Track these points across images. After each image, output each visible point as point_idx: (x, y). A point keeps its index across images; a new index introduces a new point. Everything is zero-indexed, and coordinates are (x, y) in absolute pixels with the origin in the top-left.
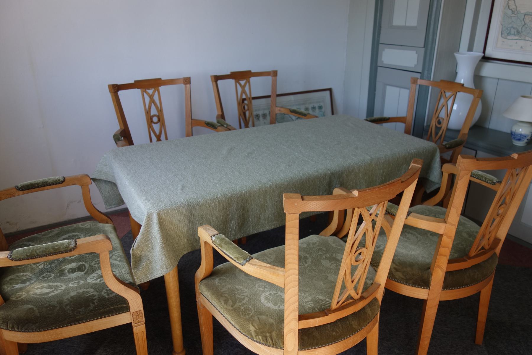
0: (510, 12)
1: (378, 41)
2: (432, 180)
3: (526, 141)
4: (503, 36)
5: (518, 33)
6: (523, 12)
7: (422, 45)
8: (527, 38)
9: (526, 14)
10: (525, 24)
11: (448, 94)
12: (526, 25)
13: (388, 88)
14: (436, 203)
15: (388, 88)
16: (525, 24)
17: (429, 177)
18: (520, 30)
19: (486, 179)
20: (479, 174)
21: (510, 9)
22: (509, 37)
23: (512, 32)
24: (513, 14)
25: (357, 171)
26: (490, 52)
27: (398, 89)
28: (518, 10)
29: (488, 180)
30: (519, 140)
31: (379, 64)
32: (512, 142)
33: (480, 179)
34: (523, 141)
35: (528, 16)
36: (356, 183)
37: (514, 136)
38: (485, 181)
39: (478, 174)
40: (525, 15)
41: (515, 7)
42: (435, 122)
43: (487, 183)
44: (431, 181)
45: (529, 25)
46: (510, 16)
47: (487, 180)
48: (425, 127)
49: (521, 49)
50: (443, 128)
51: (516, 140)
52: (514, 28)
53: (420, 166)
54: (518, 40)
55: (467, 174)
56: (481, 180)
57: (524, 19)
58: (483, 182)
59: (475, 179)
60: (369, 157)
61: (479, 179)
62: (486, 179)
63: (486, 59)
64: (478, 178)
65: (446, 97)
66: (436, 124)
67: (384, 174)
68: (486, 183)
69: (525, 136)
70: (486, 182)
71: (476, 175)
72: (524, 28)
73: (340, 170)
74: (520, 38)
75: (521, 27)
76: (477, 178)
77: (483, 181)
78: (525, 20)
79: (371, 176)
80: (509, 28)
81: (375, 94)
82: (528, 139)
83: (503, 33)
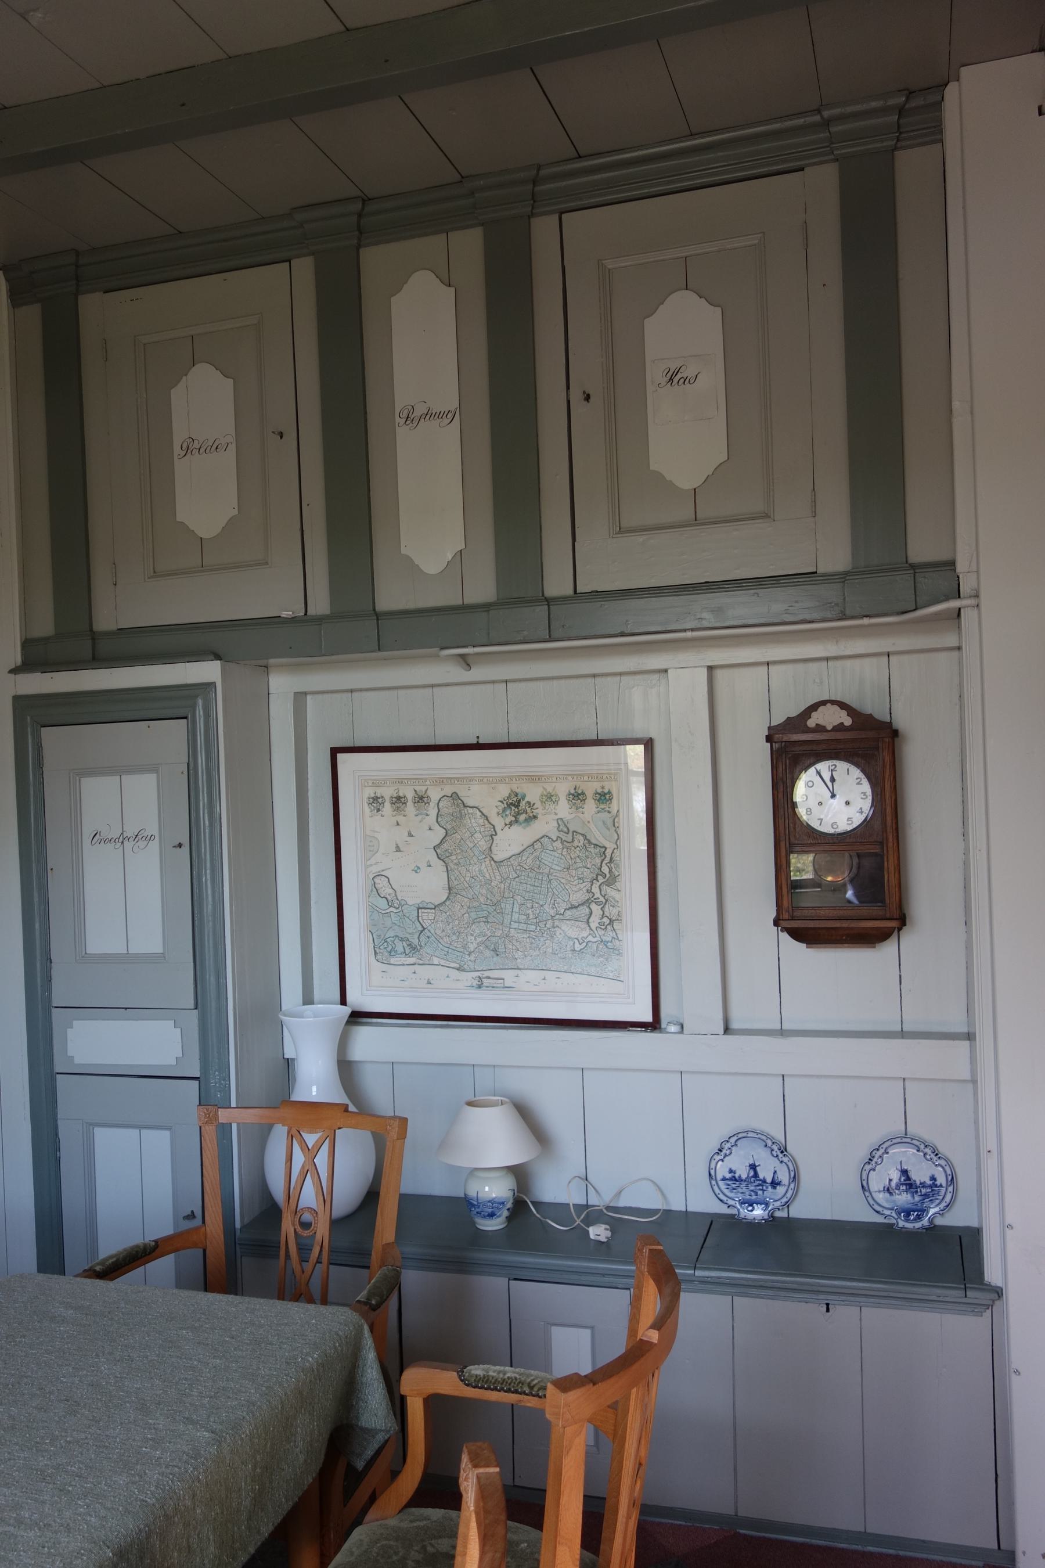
0: (382, 904)
1: (49, 999)
2: (368, 1426)
3: (506, 1213)
4: (378, 957)
5: (413, 948)
6: (413, 901)
7: (192, 1005)
8: (436, 961)
9: (421, 906)
10: (424, 929)
11: (311, 1139)
12: (426, 931)
13: (101, 1135)
14: (405, 1500)
15: (101, 1135)
16: (424, 929)
17: (358, 1419)
18: (415, 941)
19: (531, 1388)
20: (508, 1378)
21: (382, 896)
22: (393, 961)
23: (400, 949)
24: (391, 906)
25: (188, 1503)
26: (359, 998)
27: (134, 1133)
28: (400, 899)
29: (538, 1390)
30: (492, 1215)
31: (58, 1069)
32: (474, 1223)
33: (516, 1392)
34: (499, 1216)
35: (426, 911)
36: (189, 1547)
37: (477, 1210)
38: (530, 1394)
39: (506, 1377)
40: (418, 909)
41: (391, 891)
42: (293, 1225)
43: (536, 1399)
44: (362, 1429)
45: (432, 931)
46: (387, 911)
47: (536, 1389)
48: (238, 1233)
49: (429, 986)
50: (319, 1237)
51: (484, 1217)
52: (402, 940)
53: (497, 1470)
54: (417, 966)
55: (580, 1433)
56: (520, 1394)
57: (418, 916)
58: (525, 1396)
59: (502, 1394)
60: (207, 1434)
61: (513, 1392)
62: (531, 1388)
63: (357, 1017)
64: (509, 1391)
65: (309, 1149)
66: (295, 1230)
67: (258, 1470)
68: (535, 1398)
69: (503, 1203)
70: (534, 1396)
71: (502, 1384)
72: (422, 938)
73: (142, 1526)
74: (421, 962)
75: (416, 936)
76: (506, 1392)
77: (525, 1393)
78: (420, 919)
79: (227, 1496)
80: (388, 940)
81: (58, 1161)
82: (508, 1209)
83: (378, 951)
